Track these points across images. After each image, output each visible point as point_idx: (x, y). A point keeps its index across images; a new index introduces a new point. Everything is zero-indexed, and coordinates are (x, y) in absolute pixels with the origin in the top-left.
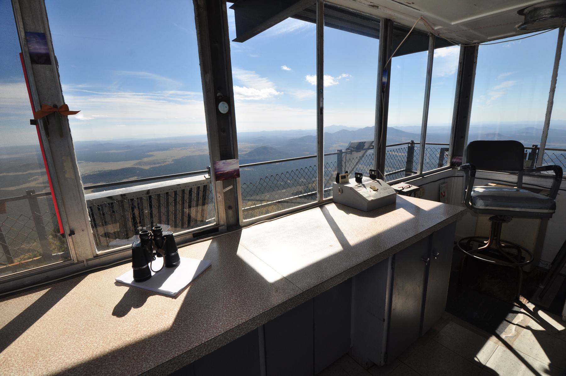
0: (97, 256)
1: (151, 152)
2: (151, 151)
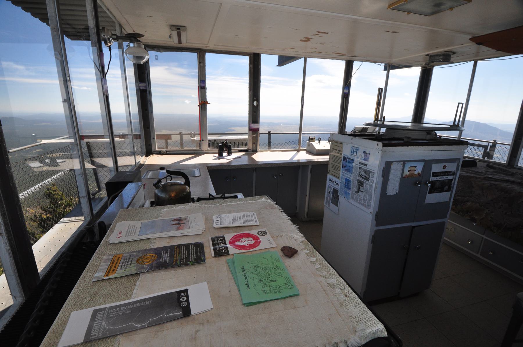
0: (208, 150)
1: (233, 127)
2: (233, 126)
